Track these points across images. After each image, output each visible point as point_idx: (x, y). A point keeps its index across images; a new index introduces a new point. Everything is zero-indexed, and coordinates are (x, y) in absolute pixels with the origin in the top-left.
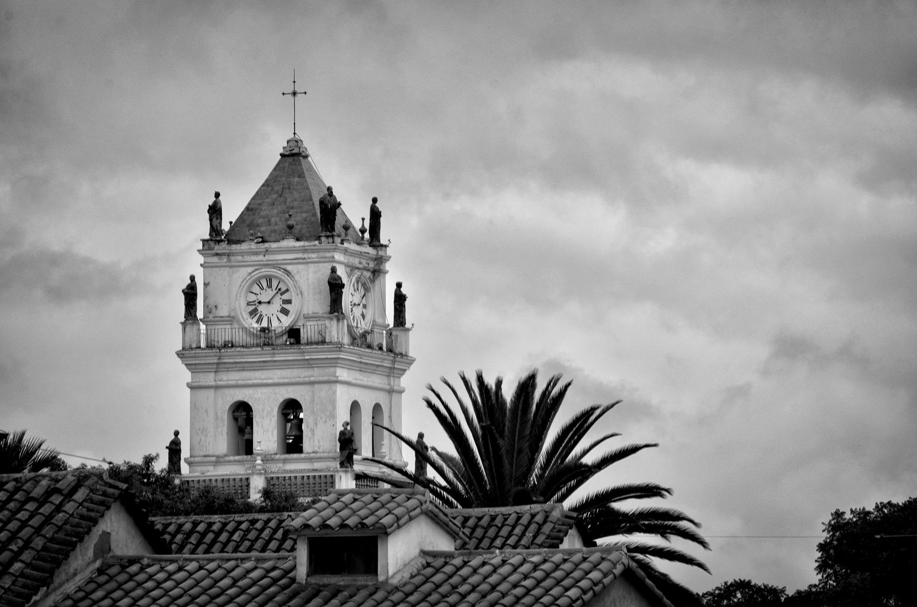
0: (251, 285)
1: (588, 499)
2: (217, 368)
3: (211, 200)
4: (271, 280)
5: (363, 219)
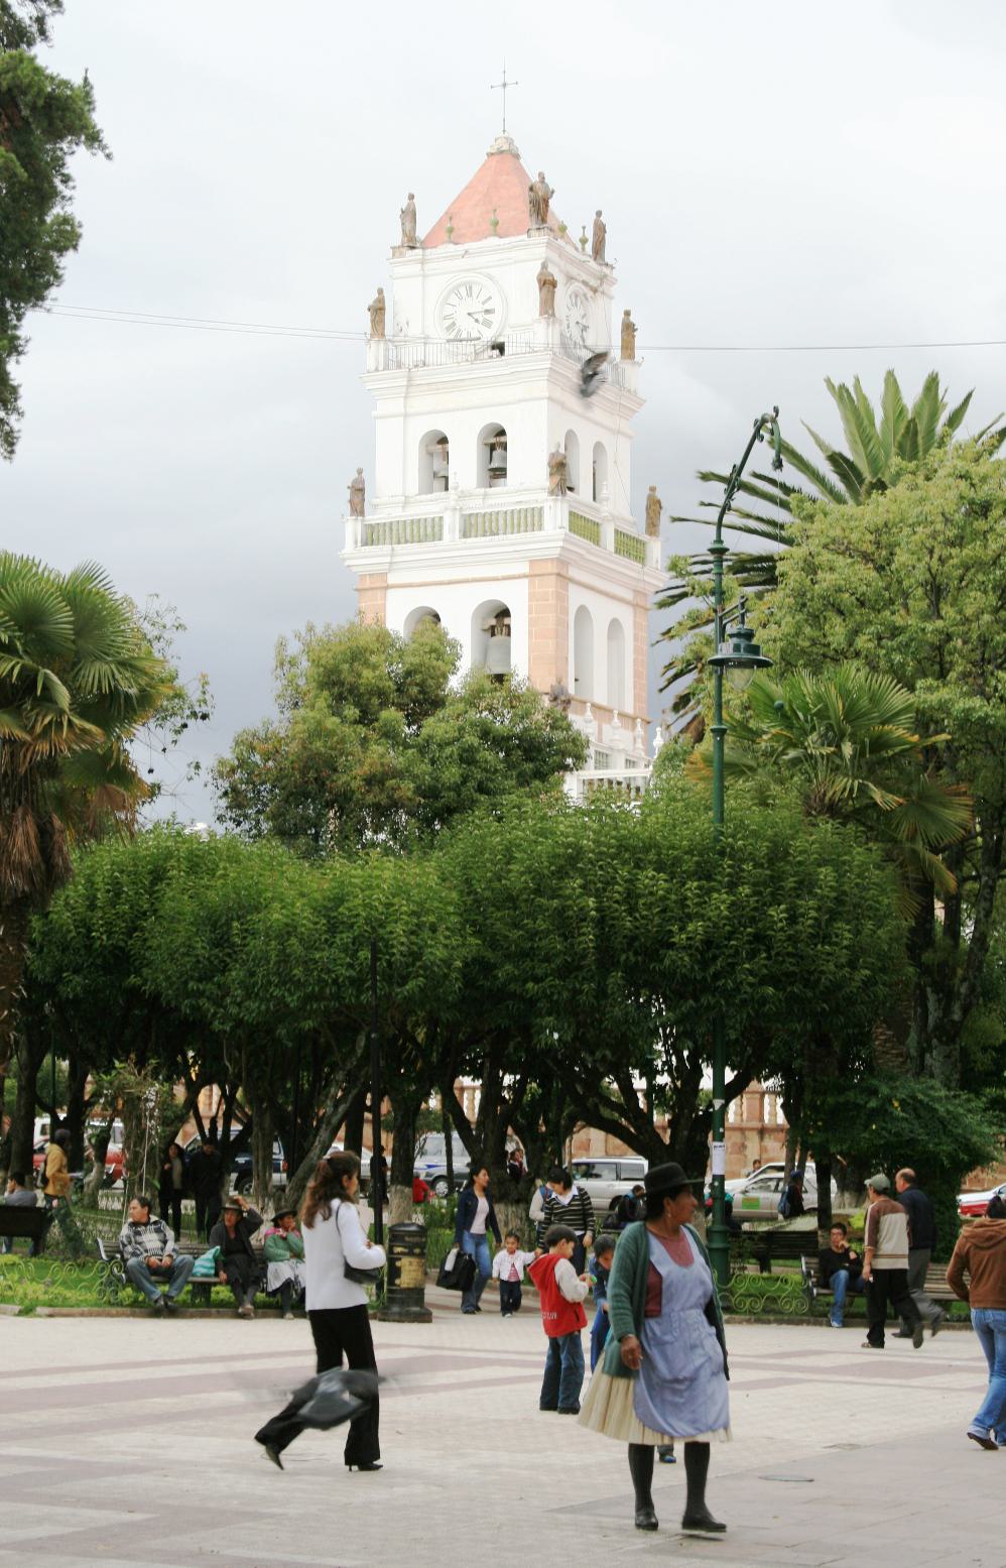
0: (449, 294)
1: (77, 579)
2: (407, 393)
3: (404, 203)
4: (471, 288)
5: (584, 228)
